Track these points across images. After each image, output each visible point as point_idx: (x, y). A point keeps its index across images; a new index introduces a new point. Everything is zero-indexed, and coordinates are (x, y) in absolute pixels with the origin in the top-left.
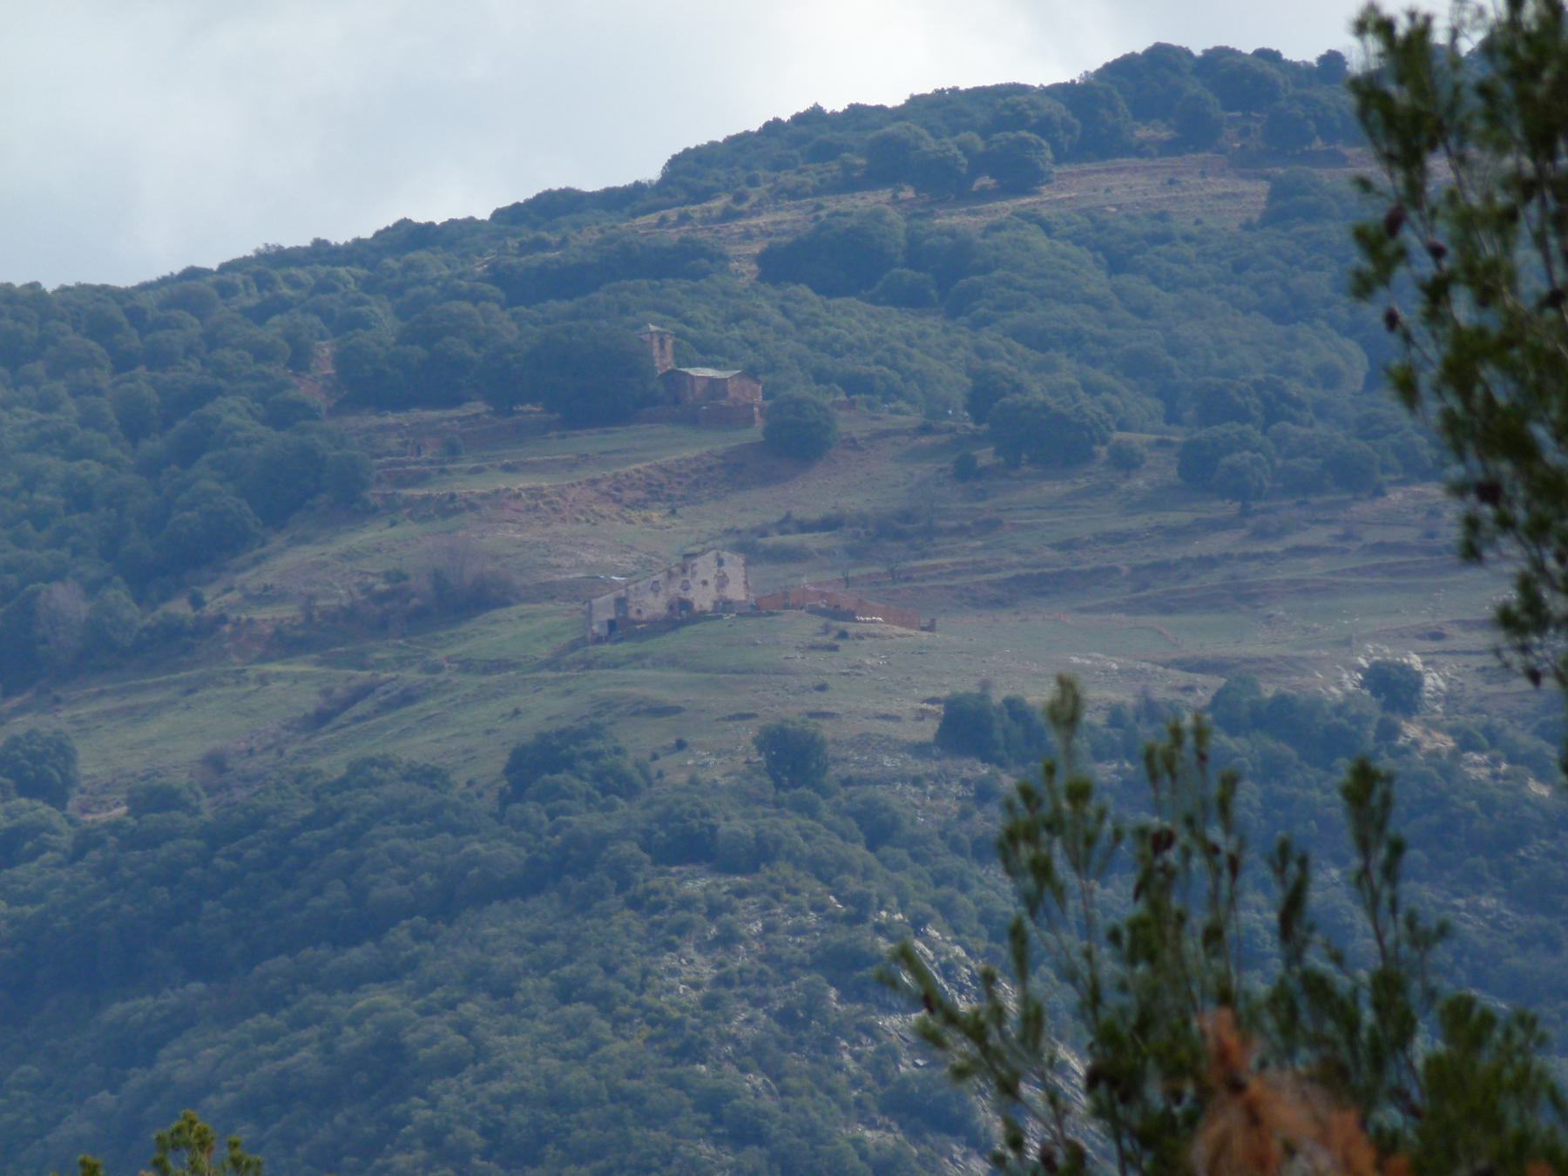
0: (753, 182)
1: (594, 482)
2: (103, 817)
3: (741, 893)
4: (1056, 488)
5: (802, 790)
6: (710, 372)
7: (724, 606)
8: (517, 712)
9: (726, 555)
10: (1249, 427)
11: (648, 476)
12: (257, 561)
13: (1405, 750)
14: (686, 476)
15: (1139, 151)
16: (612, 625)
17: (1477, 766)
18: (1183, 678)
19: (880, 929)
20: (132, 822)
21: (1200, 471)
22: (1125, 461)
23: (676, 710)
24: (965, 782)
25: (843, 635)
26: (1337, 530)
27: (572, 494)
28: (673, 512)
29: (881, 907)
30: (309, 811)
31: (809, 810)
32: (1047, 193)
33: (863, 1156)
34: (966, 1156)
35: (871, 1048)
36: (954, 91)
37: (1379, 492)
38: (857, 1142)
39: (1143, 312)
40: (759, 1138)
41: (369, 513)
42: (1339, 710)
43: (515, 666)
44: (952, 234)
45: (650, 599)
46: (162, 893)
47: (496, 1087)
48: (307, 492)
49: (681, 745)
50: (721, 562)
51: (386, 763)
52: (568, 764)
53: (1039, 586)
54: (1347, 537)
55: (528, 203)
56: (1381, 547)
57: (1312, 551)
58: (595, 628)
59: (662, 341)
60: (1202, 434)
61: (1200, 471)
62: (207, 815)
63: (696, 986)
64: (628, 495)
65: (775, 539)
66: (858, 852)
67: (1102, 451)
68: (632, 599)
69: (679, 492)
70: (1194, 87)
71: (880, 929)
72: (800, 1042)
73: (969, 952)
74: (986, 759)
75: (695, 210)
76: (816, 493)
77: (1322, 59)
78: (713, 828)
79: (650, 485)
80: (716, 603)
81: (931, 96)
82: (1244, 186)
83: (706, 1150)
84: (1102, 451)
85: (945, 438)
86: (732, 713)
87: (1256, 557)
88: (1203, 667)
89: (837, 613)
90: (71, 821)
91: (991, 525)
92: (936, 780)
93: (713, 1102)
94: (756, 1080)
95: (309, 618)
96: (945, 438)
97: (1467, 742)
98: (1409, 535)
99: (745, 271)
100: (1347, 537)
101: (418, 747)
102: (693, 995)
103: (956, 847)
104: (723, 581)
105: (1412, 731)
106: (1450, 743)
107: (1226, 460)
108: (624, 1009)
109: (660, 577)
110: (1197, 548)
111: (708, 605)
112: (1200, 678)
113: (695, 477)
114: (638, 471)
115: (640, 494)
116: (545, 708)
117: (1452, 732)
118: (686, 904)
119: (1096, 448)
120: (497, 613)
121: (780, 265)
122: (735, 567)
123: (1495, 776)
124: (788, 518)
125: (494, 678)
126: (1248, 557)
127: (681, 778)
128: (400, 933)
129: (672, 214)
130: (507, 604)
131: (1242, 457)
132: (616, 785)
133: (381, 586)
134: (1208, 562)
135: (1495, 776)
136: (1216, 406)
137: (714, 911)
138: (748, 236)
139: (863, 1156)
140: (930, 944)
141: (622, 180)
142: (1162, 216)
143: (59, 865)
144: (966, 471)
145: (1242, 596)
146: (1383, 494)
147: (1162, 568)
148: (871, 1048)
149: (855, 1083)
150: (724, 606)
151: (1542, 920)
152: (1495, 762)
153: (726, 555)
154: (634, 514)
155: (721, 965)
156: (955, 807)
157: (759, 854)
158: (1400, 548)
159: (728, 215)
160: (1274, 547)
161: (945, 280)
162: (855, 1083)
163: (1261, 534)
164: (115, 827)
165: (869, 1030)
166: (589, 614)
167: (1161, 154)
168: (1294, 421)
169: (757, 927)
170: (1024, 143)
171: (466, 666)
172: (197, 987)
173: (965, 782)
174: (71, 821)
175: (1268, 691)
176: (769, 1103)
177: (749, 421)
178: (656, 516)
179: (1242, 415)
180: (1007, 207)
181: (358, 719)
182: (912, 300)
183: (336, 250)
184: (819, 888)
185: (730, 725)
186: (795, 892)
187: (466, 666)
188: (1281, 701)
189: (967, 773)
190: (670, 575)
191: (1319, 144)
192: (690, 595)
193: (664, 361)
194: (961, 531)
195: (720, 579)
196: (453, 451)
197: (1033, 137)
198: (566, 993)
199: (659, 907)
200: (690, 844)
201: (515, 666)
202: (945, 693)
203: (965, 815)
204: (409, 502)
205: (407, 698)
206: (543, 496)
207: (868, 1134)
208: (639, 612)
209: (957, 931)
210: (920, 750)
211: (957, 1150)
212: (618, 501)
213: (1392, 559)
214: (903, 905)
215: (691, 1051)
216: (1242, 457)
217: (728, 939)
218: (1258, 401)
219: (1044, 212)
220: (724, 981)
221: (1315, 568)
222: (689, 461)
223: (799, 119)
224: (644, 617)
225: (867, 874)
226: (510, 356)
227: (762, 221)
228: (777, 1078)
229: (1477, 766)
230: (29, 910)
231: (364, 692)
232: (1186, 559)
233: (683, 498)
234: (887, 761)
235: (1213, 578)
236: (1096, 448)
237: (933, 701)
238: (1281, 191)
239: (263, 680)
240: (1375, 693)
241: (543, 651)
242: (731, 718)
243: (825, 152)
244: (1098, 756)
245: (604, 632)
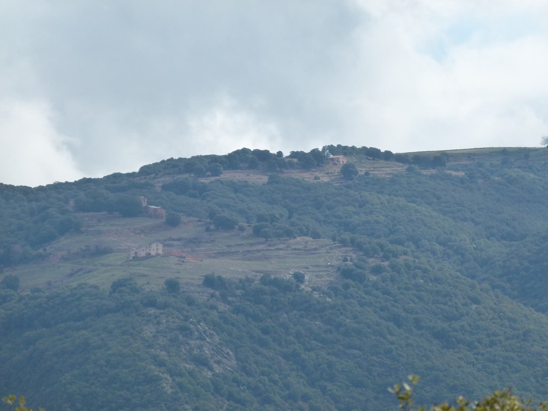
0: (160, 171)
2: (25, 294)
3: (162, 314)
4: (226, 234)
5: (174, 293)
6: (154, 207)
7: (158, 255)
8: (113, 275)
10: (268, 223)
12: (58, 242)
13: (301, 291)
15: (241, 169)
16: (134, 257)
17: (316, 295)
18: (254, 274)
19: (191, 323)
20: (31, 295)
21: (257, 232)
22: (242, 229)
23: (148, 276)
24: (208, 293)
25: (183, 262)
26: (286, 245)
29: (191, 318)
30: (69, 294)
31: (175, 297)
32: (222, 176)
33: (186, 370)
34: (207, 371)
35: (188, 347)
36: (201, 156)
37: (295, 238)
38: (185, 367)
39: (242, 201)
40: (165, 365)
42: (288, 281)
43: (113, 265)
44: (202, 183)
47: (108, 352)
48: (68, 228)
49: (148, 283)
50: (157, 246)
51: (86, 284)
52: (125, 285)
53: (223, 254)
54: (288, 247)
55: (111, 175)
56: (295, 249)
57: (281, 249)
60: (257, 224)
61: (257, 232)
62: (47, 294)
63: (151, 333)
65: (167, 242)
66: (186, 306)
67: (237, 227)
70: (250, 156)
71: (191, 323)
72: (173, 346)
73: (209, 329)
74: (213, 289)
75: (147, 177)
76: (175, 233)
77: (278, 153)
78: (156, 300)
81: (189, 159)
82: (262, 177)
83: (153, 367)
84: (237, 227)
85: (204, 223)
87: (269, 250)
88: (258, 272)
89: (181, 257)
90: (18, 294)
91: (213, 241)
92: (202, 292)
93: (155, 358)
94: (163, 353)
96: (204, 223)
97: (314, 289)
98: (301, 247)
99: (159, 190)
100: (288, 247)
101: (92, 281)
103: (206, 307)
104: (157, 249)
105: (303, 286)
106: (311, 290)
107: (263, 230)
108: (137, 337)
110: (255, 248)
111: (154, 254)
112: (258, 274)
116: (119, 274)
117: (311, 287)
118: (150, 315)
120: (109, 255)
121: (165, 188)
122: (160, 247)
123: (320, 297)
124: (170, 238)
125: (109, 268)
126: (266, 250)
127: (149, 290)
129: (143, 177)
130: (111, 253)
131: (267, 229)
132: (135, 290)
133: (84, 248)
134: (259, 251)
135: (320, 297)
136: (260, 218)
137: (156, 317)
138: (159, 182)
139: (186, 370)
140: (201, 326)
141: (130, 171)
142: (246, 182)
143: (15, 303)
144: (208, 230)
145: (267, 258)
147: (248, 251)
148: (188, 347)
149: (185, 354)
150: (158, 255)
151: (329, 327)
152: (320, 294)
153: (158, 244)
156: (206, 298)
157: (165, 306)
158: (299, 249)
159: (154, 178)
160: (273, 248)
161: (202, 192)
162: (185, 354)
163: (270, 245)
164: (28, 295)
165: (188, 344)
166: (129, 255)
168: (277, 222)
169: (164, 321)
170: (217, 166)
171: (103, 265)
172: (44, 329)
174: (18, 294)
175: (273, 277)
176: (166, 358)
177: (162, 218)
178: (142, 236)
179: (266, 220)
180: (213, 179)
181: (80, 275)
182: (194, 196)
183: (71, 183)
184: (177, 313)
186: (173, 314)
187: (103, 265)
188: (275, 279)
189: (209, 291)
190: (147, 248)
191: (278, 169)
192: (150, 252)
193: (144, 204)
194: (207, 242)
195: (157, 249)
196: (99, 221)
197: (219, 164)
199: (144, 316)
200: (152, 304)
201: (113, 265)
202: (204, 274)
203: (208, 300)
205: (90, 271)
207: (187, 365)
209: (207, 324)
210: (199, 286)
211: (206, 369)
213: (297, 252)
214: (195, 318)
215: (150, 346)
216: (267, 229)
217: (159, 323)
219: (222, 180)
220: (158, 332)
221: (281, 252)
223: (168, 160)
225: (188, 311)
227: (162, 179)
228: (168, 353)
229: (316, 295)
230: (9, 312)
231: (81, 270)
234: (192, 288)
235: (259, 254)
237: (202, 276)
238: (271, 178)
239: (59, 267)
240: (295, 279)
241: (119, 263)
243: (174, 166)
244: (237, 289)
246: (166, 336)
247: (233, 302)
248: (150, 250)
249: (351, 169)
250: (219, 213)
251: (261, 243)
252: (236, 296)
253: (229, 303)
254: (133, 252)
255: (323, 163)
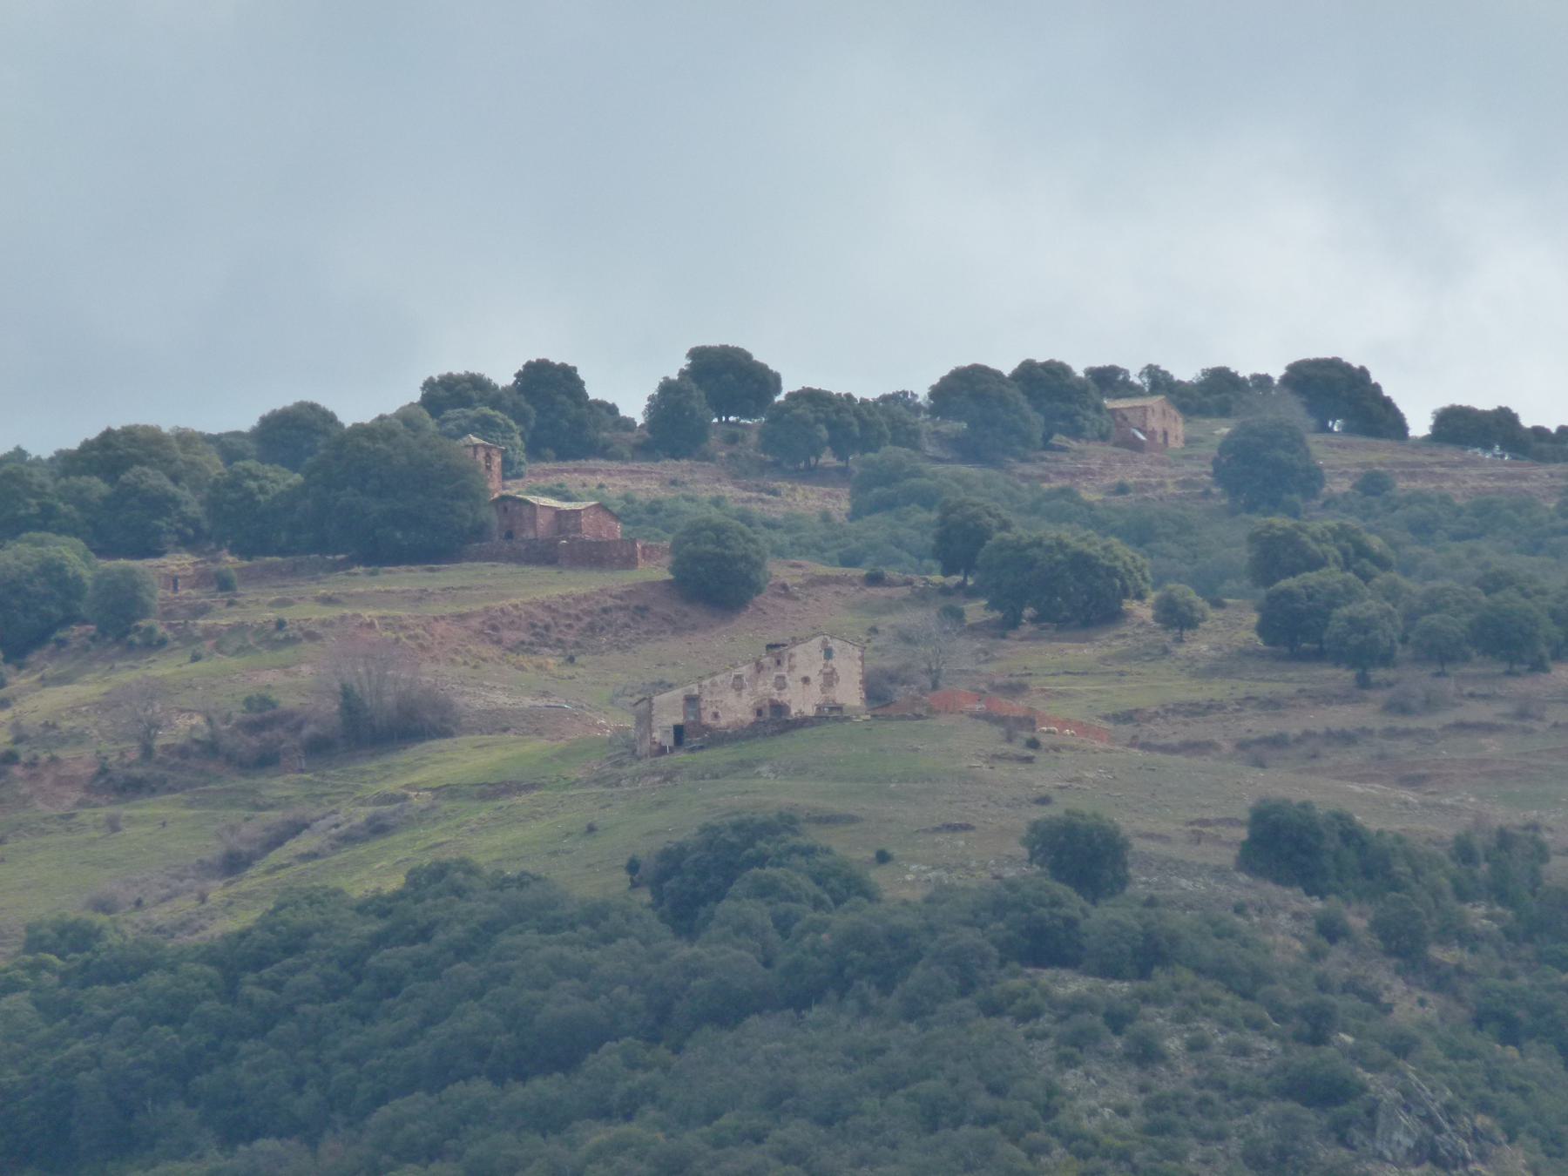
1: (461, 617)
8: (591, 829)
9: (835, 644)
11: (531, 615)
14: (578, 618)
16: (679, 731)
23: (852, 819)
24: (1297, 916)
27: (440, 628)
28: (571, 659)
41: (154, 645)
43: (533, 787)
45: (730, 698)
46: (166, 1033)
50: (828, 653)
57: (1489, 728)
58: (657, 735)
59: (488, 457)
63: (1123, 1112)
64: (510, 636)
68: (707, 698)
69: (570, 638)
79: (534, 626)
80: (819, 708)
86: (937, 824)
87: (1407, 733)
95: (147, 752)
102: (1124, 1124)
104: (830, 678)
109: (745, 670)
111: (810, 711)
113: (587, 619)
114: (516, 607)
115: (525, 636)
119: (1130, 605)
128: (608, 1057)
137: (1117, 1021)
146: (1546, 670)
154: (523, 659)
155: (1143, 1089)
167: (633, 459)
173: (1297, 916)
185: (939, 838)
190: (759, 667)
191: (828, 459)
192: (785, 697)
198: (933, 1117)
204: (209, 633)
206: (403, 627)
208: (716, 715)
210: (1219, 872)
212: (499, 642)
217: (1146, 1054)
218: (1337, 553)
221: (1493, 746)
222: (577, 600)
224: (723, 722)
226: (252, 484)
232: (1308, 734)
233: (577, 644)
236: (1130, 605)
242: (937, 830)
244: (1462, 895)
245: (669, 741)
246: (1220, 1136)
247: (1459, 970)
248: (781, 684)
249: (1282, 454)
250: (1005, 526)
251: (1327, 698)
252: (1470, 940)
253: (1442, 981)
254: (678, 694)
255: (1076, 433)
